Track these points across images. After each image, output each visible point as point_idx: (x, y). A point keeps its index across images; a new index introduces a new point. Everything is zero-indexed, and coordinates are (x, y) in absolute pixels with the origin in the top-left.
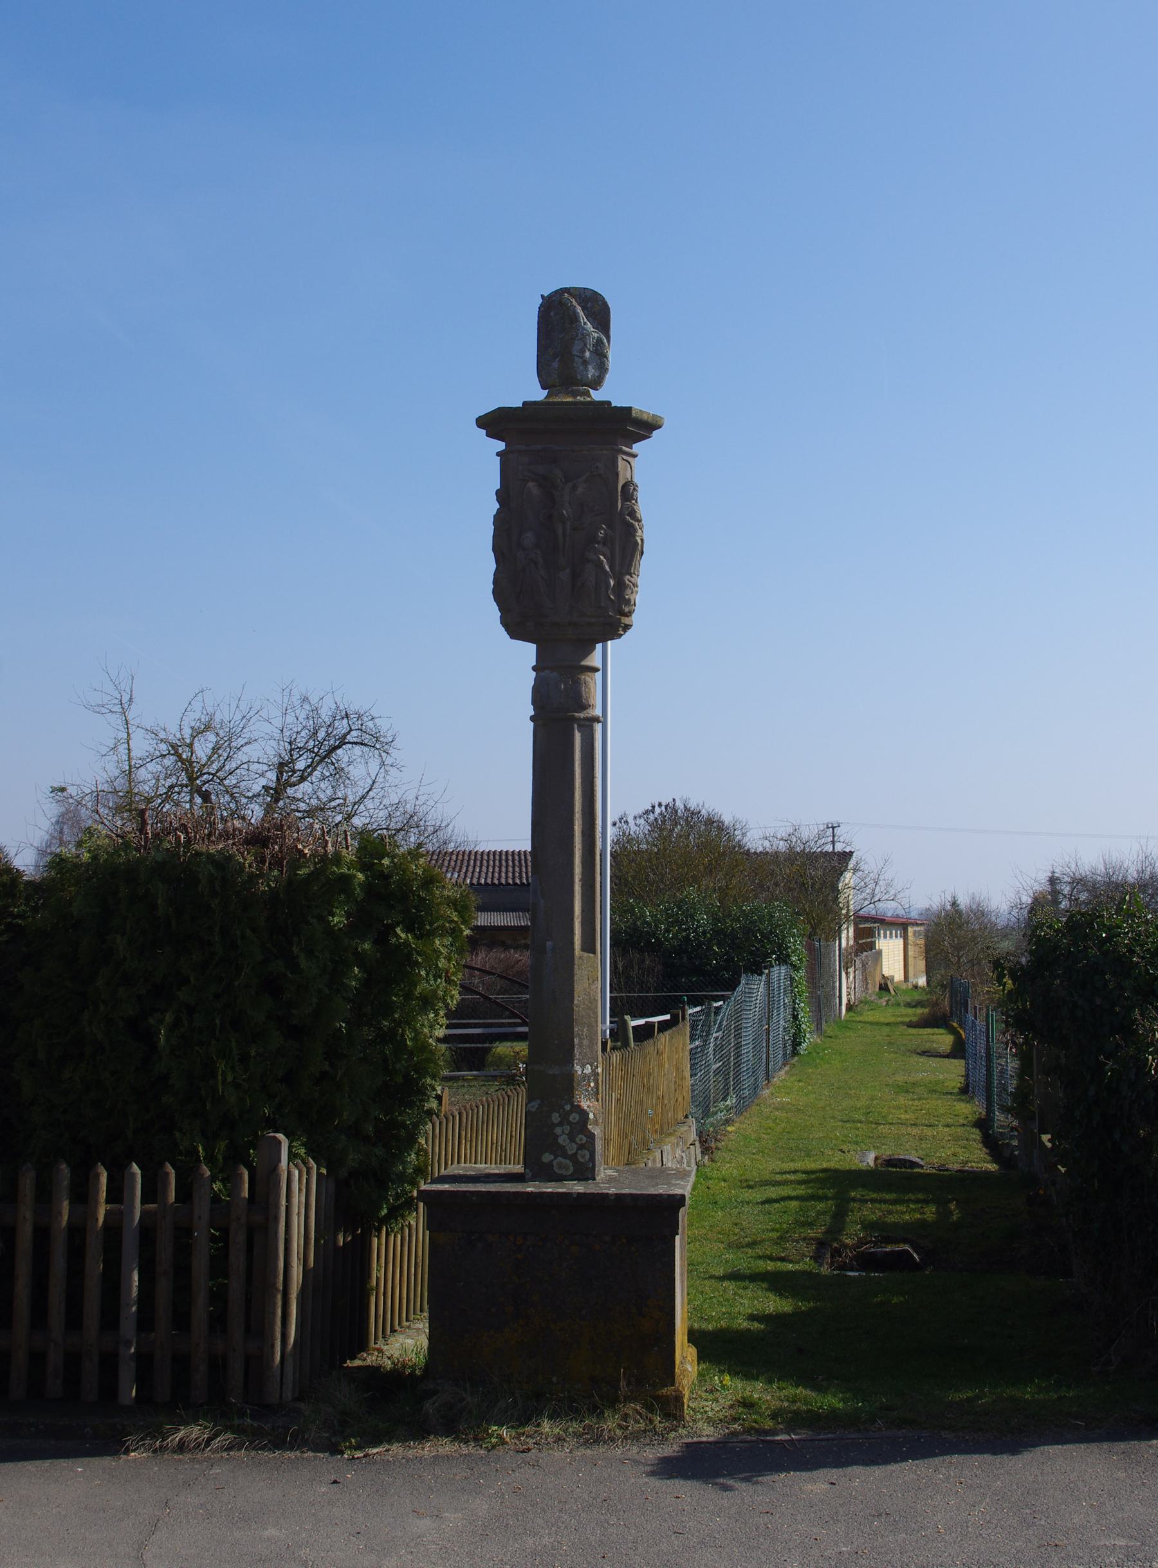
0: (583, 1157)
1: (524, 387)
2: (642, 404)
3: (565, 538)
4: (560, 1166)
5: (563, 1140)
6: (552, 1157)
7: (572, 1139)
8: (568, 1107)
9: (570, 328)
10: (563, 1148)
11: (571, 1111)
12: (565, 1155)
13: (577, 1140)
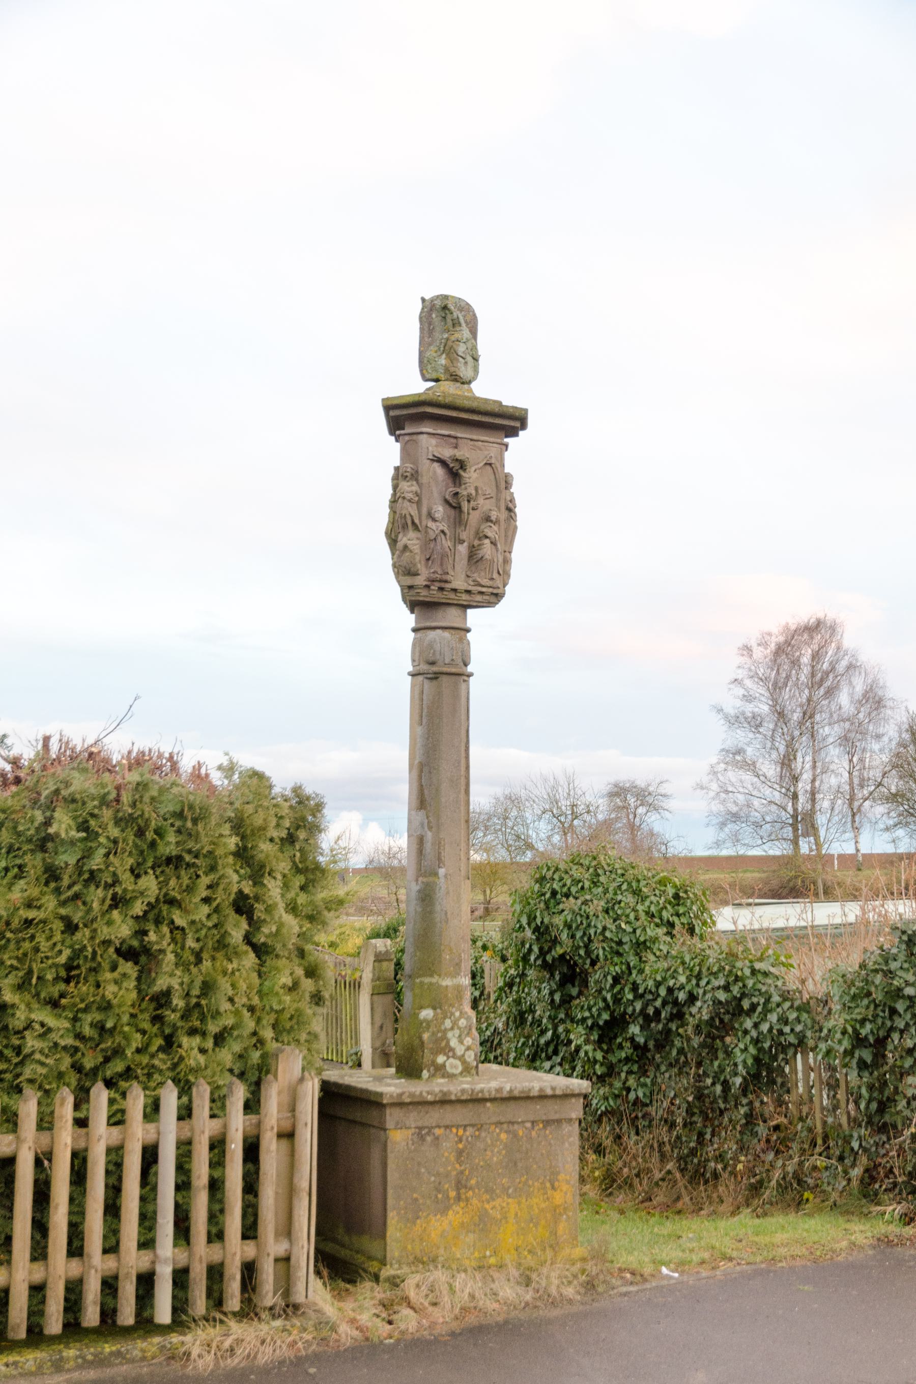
0: (470, 1057)
1: (412, 384)
2: (510, 399)
3: (735, 923)
4: (452, 1066)
5: (454, 1043)
6: (445, 1058)
7: (461, 1042)
8: (457, 1014)
9: (446, 325)
10: (452, 1050)
11: (460, 1017)
12: (454, 1057)
13: (465, 1042)
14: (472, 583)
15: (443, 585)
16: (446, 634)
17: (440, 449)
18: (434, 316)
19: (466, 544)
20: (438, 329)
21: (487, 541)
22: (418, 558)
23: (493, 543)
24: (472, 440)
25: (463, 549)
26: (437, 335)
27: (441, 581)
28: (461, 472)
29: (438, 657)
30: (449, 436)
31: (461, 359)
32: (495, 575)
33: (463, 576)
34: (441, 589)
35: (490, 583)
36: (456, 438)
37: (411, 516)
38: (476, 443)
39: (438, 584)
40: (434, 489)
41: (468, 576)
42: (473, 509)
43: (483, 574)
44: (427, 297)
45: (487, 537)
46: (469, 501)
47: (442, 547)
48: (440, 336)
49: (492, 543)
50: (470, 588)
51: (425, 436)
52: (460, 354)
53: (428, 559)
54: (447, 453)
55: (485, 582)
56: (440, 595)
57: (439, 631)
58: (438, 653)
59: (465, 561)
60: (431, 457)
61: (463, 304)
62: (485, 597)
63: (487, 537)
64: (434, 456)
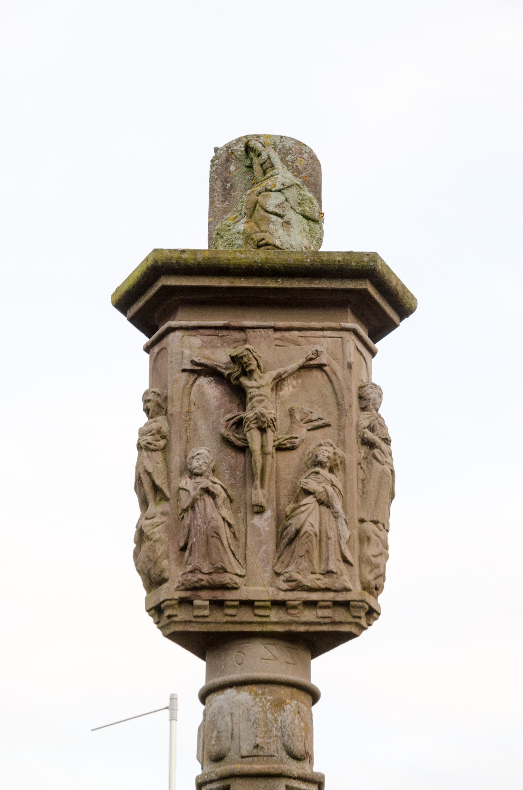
14: (285, 586)
15: (220, 595)
16: (244, 696)
17: (207, 352)
18: (232, 168)
19: (269, 513)
20: (240, 186)
21: (310, 499)
22: (160, 549)
23: (324, 503)
24: (276, 329)
25: (264, 523)
26: (237, 194)
27: (213, 587)
28: (245, 381)
29: (226, 743)
30: (226, 328)
31: (274, 218)
32: (335, 565)
33: (268, 575)
34: (218, 604)
35: (325, 582)
36: (243, 329)
37: (149, 474)
38: (287, 334)
39: (206, 594)
40: (201, 423)
41: (278, 574)
42: (280, 448)
43: (305, 564)
44: (220, 145)
45: (308, 493)
46: (263, 430)
47: (207, 521)
48: (243, 198)
49: (321, 503)
50: (281, 596)
51: (178, 334)
52: (271, 209)
53: (184, 549)
54: (220, 356)
55: (309, 580)
56: (219, 616)
57: (230, 692)
58: (225, 735)
59: (271, 546)
60: (189, 366)
61: (288, 144)
62: (321, 613)
63: (308, 493)
64: (193, 362)
